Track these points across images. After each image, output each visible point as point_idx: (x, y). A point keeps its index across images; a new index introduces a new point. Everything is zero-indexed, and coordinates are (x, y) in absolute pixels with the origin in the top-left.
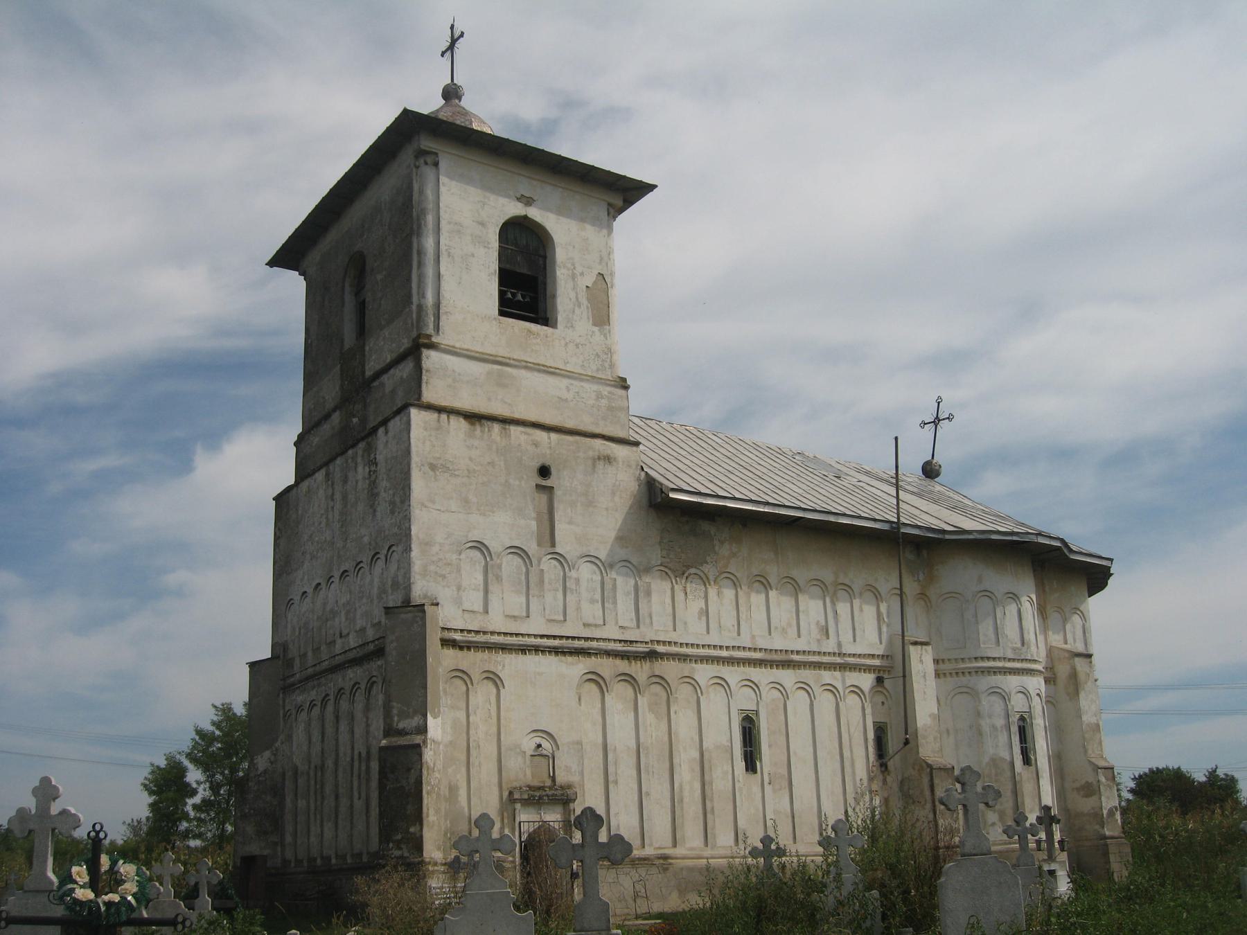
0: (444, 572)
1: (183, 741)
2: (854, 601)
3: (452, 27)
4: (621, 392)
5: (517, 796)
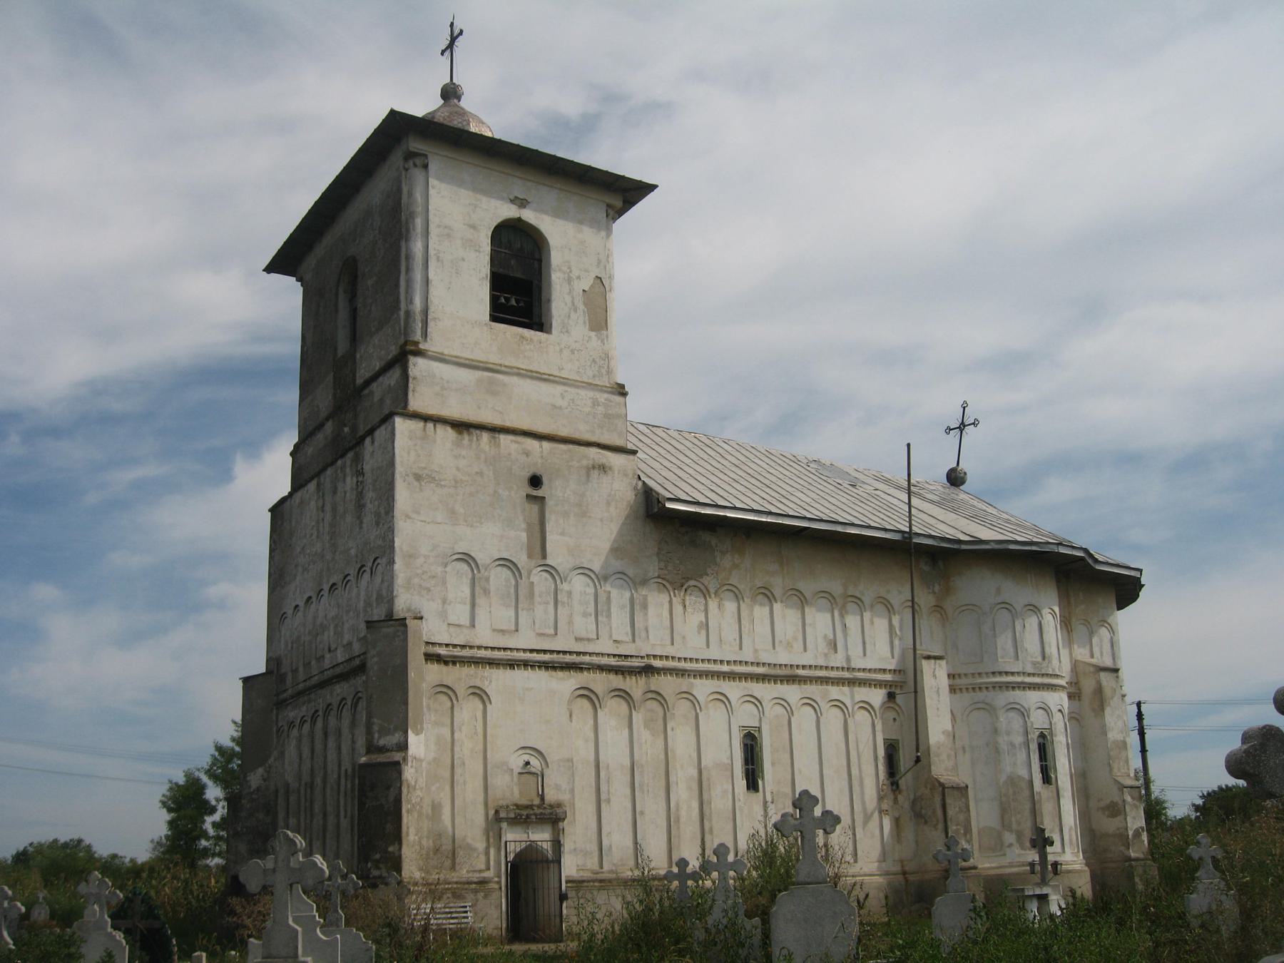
0: (428, 585)
1: (203, 759)
2: (864, 614)
3: (452, 25)
4: (619, 399)
5: (503, 815)
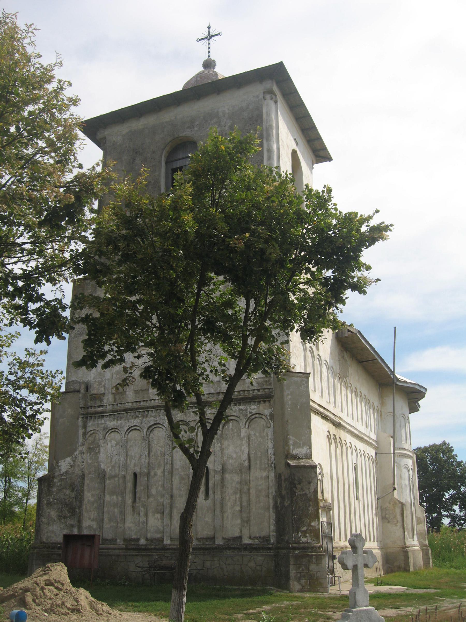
3: (209, 28)
